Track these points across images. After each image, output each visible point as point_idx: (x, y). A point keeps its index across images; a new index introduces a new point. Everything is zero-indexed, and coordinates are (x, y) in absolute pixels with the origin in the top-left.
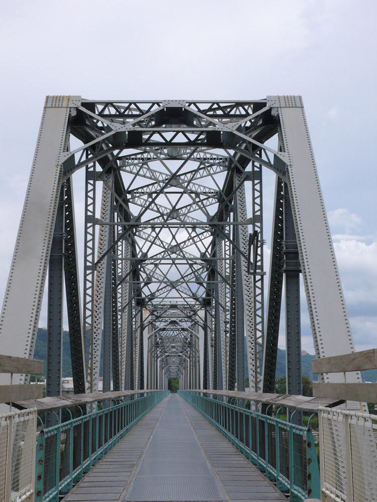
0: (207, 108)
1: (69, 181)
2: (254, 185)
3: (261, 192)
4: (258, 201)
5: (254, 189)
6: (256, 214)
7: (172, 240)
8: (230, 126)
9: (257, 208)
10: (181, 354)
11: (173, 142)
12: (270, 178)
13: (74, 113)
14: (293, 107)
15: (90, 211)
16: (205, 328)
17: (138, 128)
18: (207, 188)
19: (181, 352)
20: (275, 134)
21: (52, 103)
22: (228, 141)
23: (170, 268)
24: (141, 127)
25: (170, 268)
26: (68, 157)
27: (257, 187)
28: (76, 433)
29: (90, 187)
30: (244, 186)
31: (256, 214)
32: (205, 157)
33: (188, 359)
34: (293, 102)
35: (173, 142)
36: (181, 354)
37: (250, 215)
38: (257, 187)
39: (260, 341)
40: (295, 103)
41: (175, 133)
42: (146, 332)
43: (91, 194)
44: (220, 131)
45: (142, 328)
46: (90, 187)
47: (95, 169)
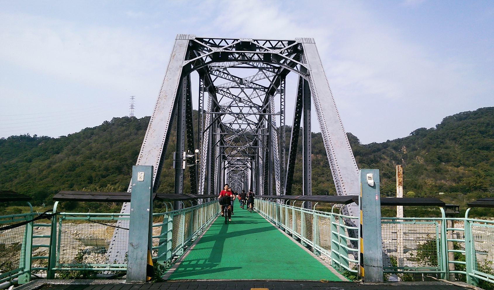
2: (281, 96)
4: (283, 100)
7: (238, 122)
10: (240, 181)
11: (220, 45)
16: (251, 169)
18: (227, 96)
19: (240, 180)
21: (182, 37)
23: (257, 119)
25: (257, 119)
30: (31, 225)
32: (267, 67)
33: (243, 183)
34: (310, 40)
35: (220, 45)
36: (240, 181)
39: (278, 159)
40: (311, 41)
41: (234, 40)
42: (226, 170)
43: (201, 98)
44: (421, 274)
46: (201, 95)
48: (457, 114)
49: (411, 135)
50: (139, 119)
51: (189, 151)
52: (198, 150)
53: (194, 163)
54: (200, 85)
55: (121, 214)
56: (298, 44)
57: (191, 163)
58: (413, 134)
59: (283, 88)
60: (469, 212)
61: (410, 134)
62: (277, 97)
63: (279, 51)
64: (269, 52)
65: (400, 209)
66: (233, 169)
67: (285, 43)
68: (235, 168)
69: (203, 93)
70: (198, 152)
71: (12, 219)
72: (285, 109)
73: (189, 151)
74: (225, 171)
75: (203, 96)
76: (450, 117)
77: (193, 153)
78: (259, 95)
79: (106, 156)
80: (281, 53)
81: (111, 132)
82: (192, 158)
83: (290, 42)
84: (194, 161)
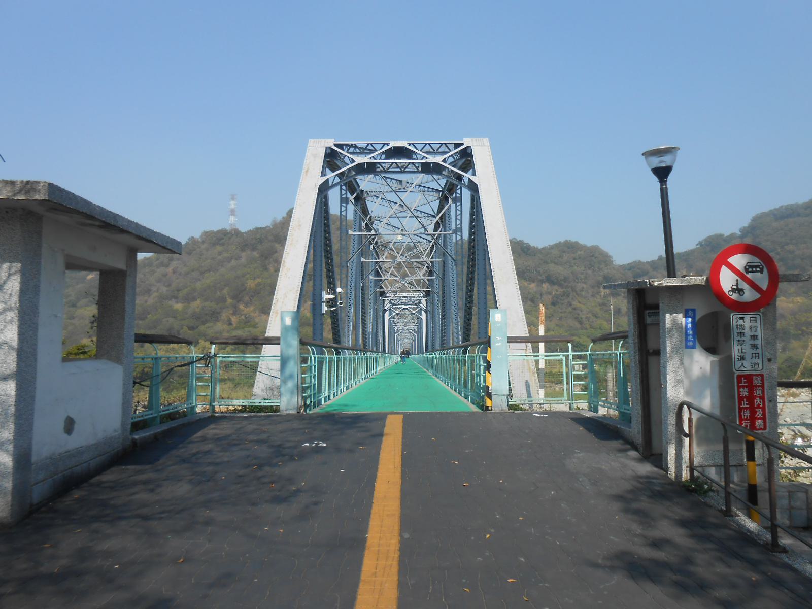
0: (425, 314)
1: (326, 198)
2: (456, 207)
3: (461, 211)
5: (456, 209)
6: (459, 204)
8: (438, 159)
9: (459, 222)
12: (467, 195)
13: (329, 151)
14: (482, 146)
15: (344, 206)
17: (373, 161)
20: (469, 170)
22: (435, 169)
24: (375, 159)
26: (326, 179)
27: (459, 208)
28: (349, 420)
29: (343, 209)
31: (459, 204)
36: (411, 331)
37: (454, 227)
38: (459, 208)
45: (384, 311)
46: (343, 209)
47: (346, 196)
48: (776, 209)
49: (699, 246)
50: (244, 233)
51: (329, 290)
52: (340, 289)
53: (336, 305)
54: (341, 195)
55: (262, 355)
56: (467, 147)
57: (333, 306)
58: (702, 245)
59: (459, 196)
60: (622, 344)
61: (697, 245)
62: (451, 205)
63: (442, 158)
64: (428, 161)
65: (542, 346)
66: (398, 312)
67: (451, 147)
68: (401, 311)
69: (346, 206)
70: (340, 291)
71: (168, 359)
72: (462, 226)
73: (329, 290)
74: (385, 315)
75: (346, 210)
76: (763, 216)
77: (334, 292)
78: (429, 201)
79: (542, 308)
80: (444, 161)
81: (201, 255)
82: (403, 469)
83: (457, 145)
84: (336, 302)
